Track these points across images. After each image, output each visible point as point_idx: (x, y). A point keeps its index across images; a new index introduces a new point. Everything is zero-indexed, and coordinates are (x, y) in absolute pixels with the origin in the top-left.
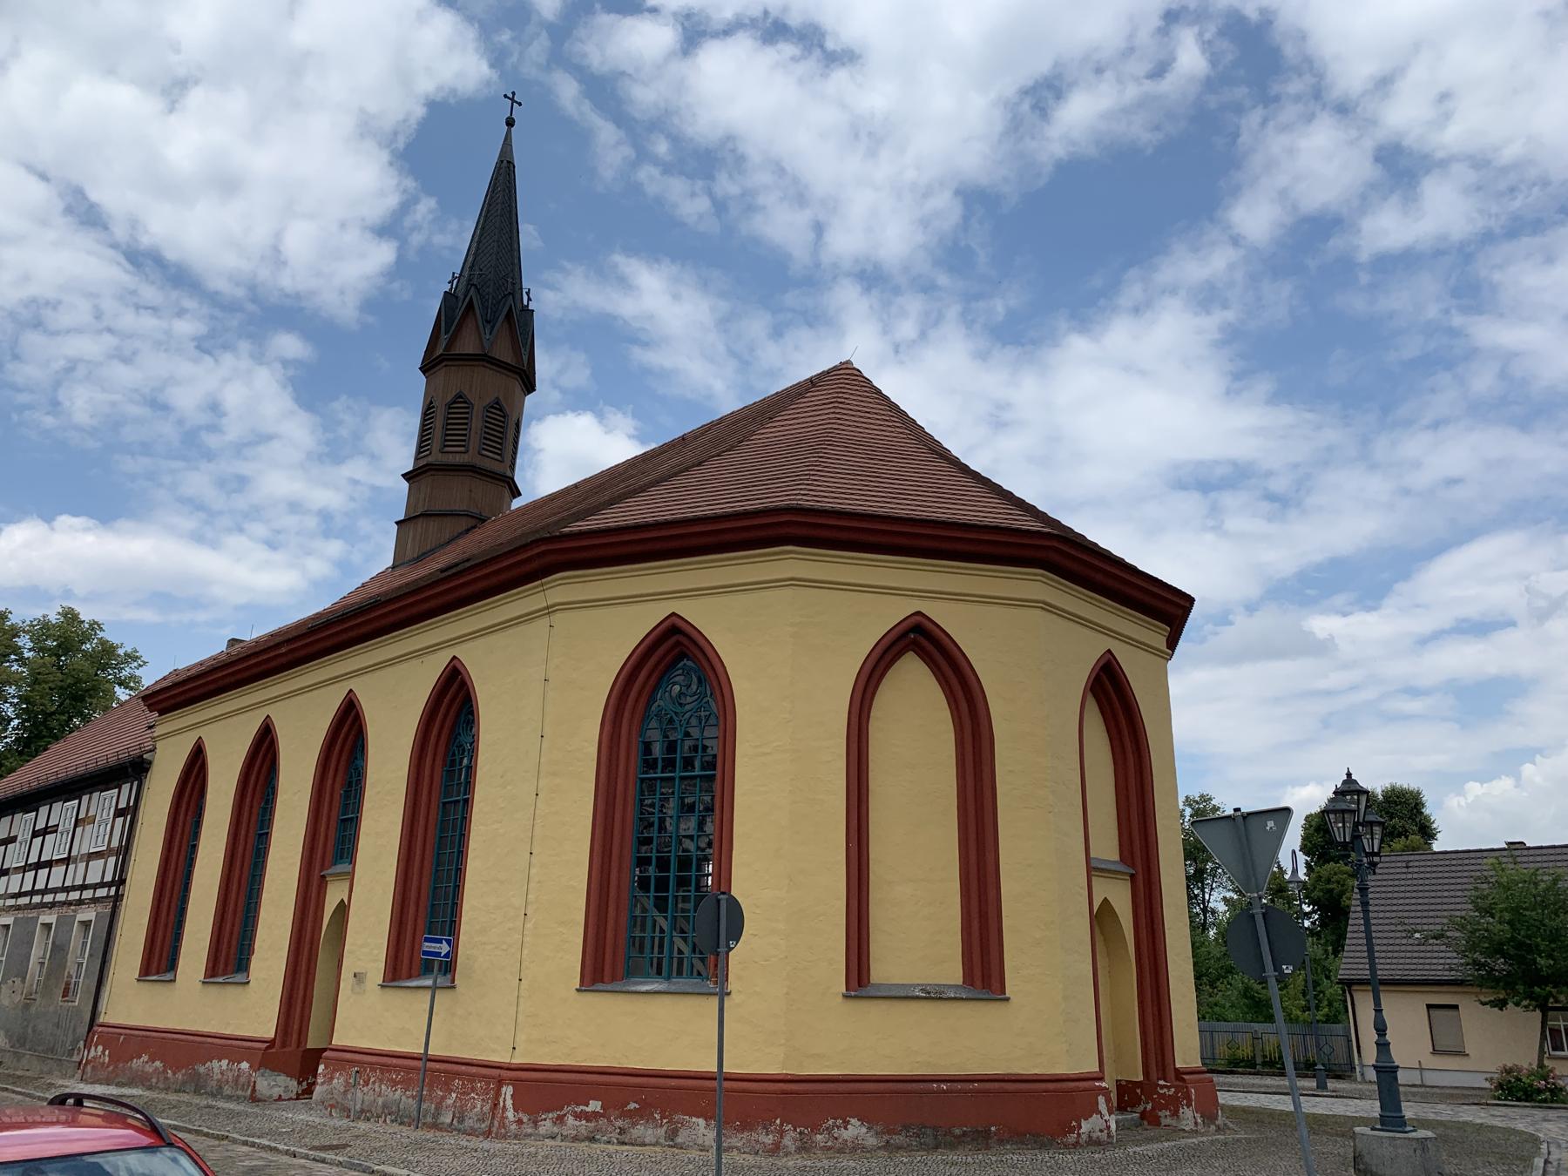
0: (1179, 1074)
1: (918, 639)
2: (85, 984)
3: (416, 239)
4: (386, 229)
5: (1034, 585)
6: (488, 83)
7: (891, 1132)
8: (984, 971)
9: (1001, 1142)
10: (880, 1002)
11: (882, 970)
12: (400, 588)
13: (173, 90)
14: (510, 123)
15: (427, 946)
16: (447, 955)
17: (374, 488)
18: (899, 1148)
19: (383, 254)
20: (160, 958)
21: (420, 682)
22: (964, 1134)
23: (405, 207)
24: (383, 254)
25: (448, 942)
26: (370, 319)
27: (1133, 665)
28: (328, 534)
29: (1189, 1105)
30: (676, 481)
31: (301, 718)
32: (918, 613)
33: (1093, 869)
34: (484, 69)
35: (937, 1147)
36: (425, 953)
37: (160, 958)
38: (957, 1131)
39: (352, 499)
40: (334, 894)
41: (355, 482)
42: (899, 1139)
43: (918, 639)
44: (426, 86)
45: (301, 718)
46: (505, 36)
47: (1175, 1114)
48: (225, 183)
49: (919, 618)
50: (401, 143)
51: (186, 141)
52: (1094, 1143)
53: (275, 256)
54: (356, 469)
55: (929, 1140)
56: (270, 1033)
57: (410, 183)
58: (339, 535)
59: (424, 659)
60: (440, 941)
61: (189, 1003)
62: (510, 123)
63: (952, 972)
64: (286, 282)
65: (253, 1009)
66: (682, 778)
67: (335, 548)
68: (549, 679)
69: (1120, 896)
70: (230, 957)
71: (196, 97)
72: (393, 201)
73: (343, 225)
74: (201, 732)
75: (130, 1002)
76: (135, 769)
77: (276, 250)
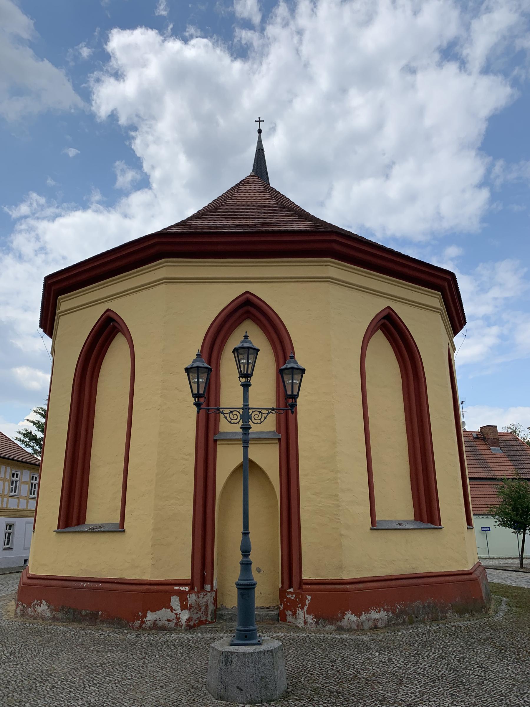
0: (302, 583)
1: (247, 309)
3: (498, 182)
4: (485, 182)
6: (512, 96)
7: (56, 610)
9: (102, 622)
10: (108, 533)
13: (386, 172)
14: (260, 131)
17: (506, 299)
18: (58, 619)
19: (485, 194)
22: (86, 615)
23: (489, 171)
24: (485, 194)
26: (485, 225)
28: (489, 325)
29: (302, 608)
32: (247, 292)
34: (508, 90)
35: (74, 621)
38: (84, 613)
39: (496, 307)
41: (495, 299)
42: (59, 615)
43: (247, 309)
44: (485, 112)
46: (516, 71)
47: (294, 614)
48: (411, 197)
49: (248, 295)
50: (479, 144)
51: (394, 189)
52: (156, 627)
53: (439, 216)
54: (495, 292)
55: (71, 617)
57: (488, 159)
58: (494, 324)
62: (260, 131)
64: (446, 225)
67: (495, 330)
71: (396, 170)
72: (481, 171)
73: (463, 191)
77: (439, 213)
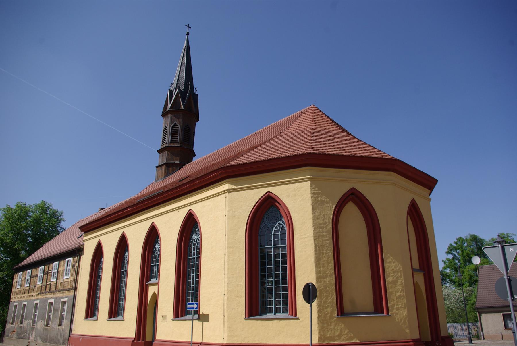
1: (354, 197)
2: (66, 322)
5: (391, 176)
8: (379, 305)
11: (347, 306)
12: (161, 188)
15: (189, 306)
16: (197, 308)
20: (91, 312)
21: (145, 227)
25: (197, 304)
27: (420, 203)
30: (263, 146)
31: (168, 222)
33: (413, 270)
36: (188, 308)
37: (91, 312)
40: (152, 290)
43: (354, 197)
45: (136, 231)
56: (134, 336)
59: (179, 210)
60: (194, 304)
61: (102, 326)
62: (188, 34)
63: (370, 305)
65: (127, 327)
66: (274, 247)
68: (222, 215)
69: (420, 279)
70: (116, 311)
74: (193, 207)
75: (82, 327)
76: (78, 252)
